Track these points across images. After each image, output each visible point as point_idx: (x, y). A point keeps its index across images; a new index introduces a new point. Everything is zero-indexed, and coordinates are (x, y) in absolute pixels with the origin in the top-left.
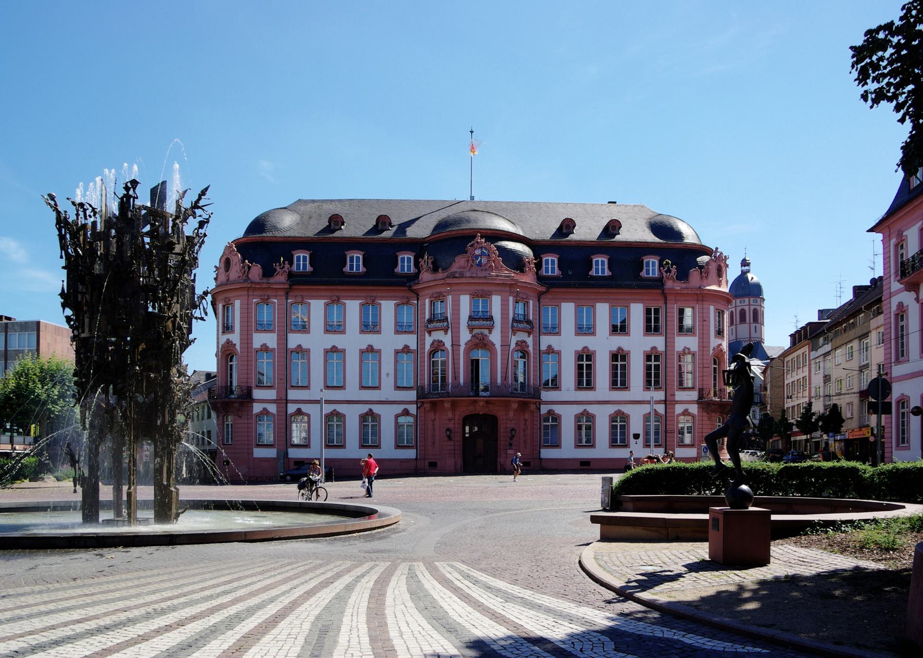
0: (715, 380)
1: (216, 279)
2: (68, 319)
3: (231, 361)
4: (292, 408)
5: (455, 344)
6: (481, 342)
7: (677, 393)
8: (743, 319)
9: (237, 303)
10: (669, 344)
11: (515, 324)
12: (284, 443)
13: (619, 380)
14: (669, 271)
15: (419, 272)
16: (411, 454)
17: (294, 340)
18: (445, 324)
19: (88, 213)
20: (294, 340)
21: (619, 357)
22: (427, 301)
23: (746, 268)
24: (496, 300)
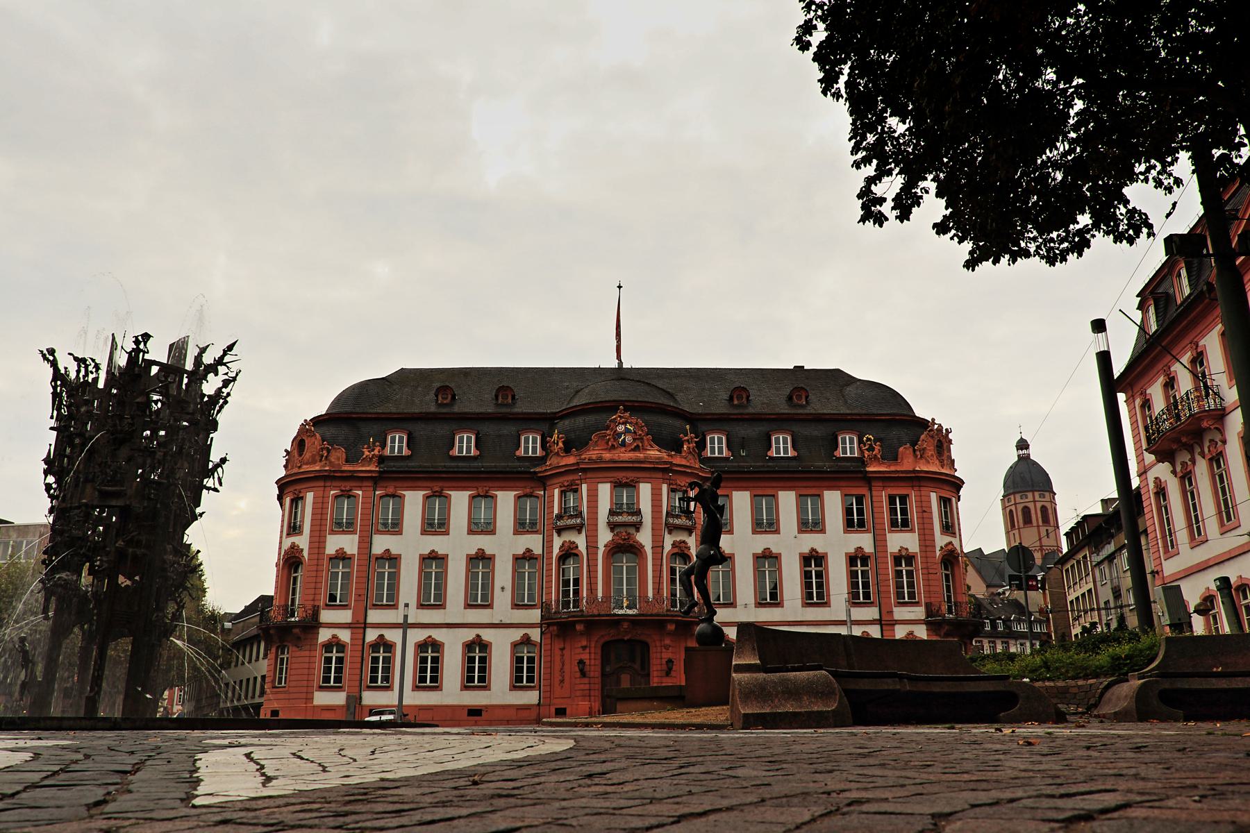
0: (949, 591)
1: (286, 467)
2: (48, 487)
3: (296, 572)
4: (371, 635)
5: (592, 546)
6: (624, 547)
7: (895, 609)
8: (1027, 520)
9: (310, 497)
10: (880, 542)
11: (671, 520)
12: (357, 683)
13: (479, 597)
14: (871, 449)
15: (547, 455)
16: (531, 697)
17: (381, 544)
18: (579, 521)
19: (90, 368)
20: (381, 544)
21: (813, 561)
22: (556, 492)
23: (1025, 451)
24: (645, 489)
